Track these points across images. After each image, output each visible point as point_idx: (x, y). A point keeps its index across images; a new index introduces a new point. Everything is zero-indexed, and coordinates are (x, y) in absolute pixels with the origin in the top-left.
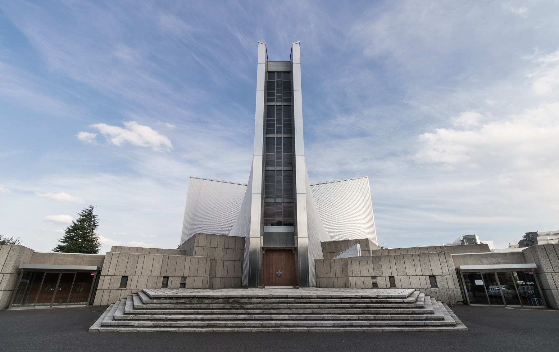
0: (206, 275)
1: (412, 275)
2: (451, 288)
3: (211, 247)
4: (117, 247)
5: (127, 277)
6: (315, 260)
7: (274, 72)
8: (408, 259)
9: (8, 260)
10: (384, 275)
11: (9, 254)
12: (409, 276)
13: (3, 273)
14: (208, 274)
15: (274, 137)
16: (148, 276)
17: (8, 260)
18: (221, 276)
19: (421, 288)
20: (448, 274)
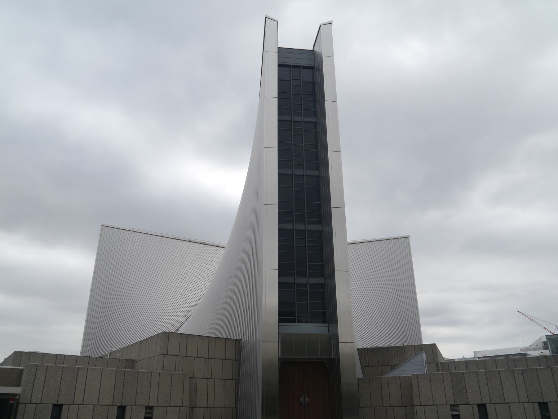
1: (513, 401)
4: (22, 353)
10: (469, 403)
12: (508, 403)
16: (94, 405)
20: (519, 402)
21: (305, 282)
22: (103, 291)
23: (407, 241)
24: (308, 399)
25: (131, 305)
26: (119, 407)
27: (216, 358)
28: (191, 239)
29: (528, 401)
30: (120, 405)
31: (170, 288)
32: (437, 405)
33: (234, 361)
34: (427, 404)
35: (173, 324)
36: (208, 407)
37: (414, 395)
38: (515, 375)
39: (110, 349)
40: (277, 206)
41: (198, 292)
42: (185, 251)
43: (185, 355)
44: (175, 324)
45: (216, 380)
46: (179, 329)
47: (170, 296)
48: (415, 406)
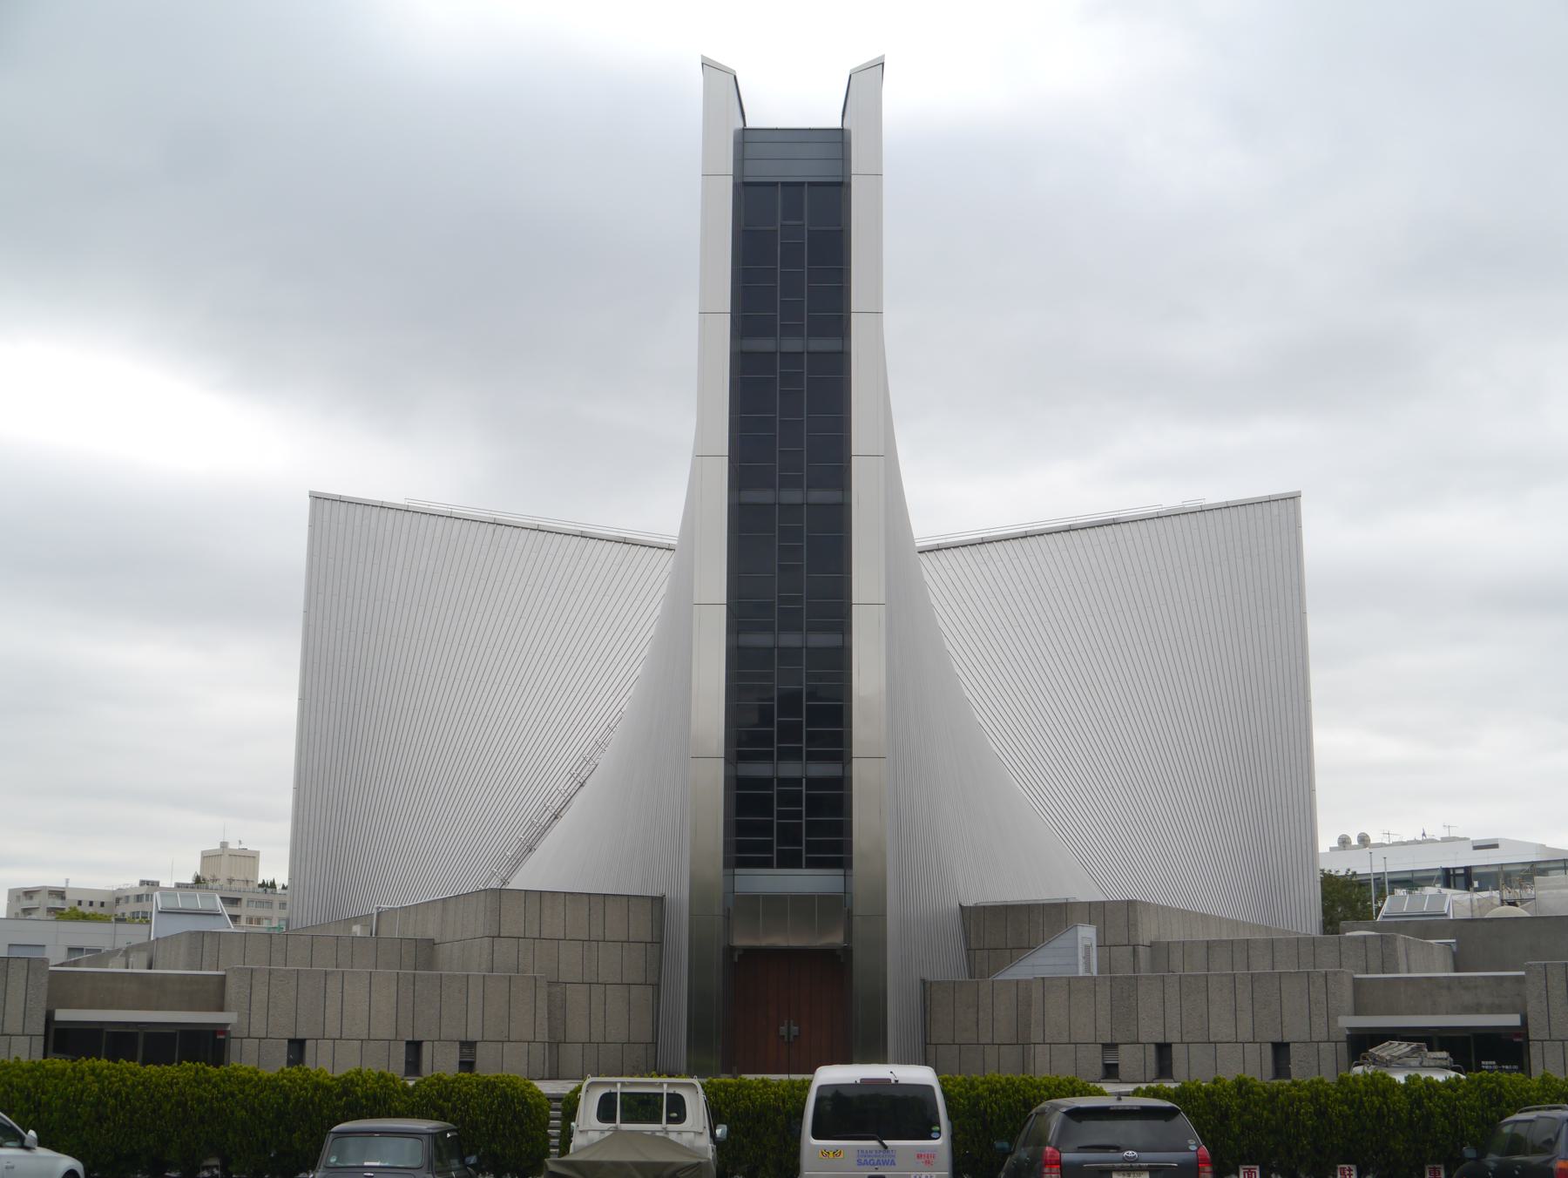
0: (537, 1035)
3: (542, 937)
5: (1288, 1045)
6: (924, 982)
7: (802, 184)
9: (31, 1001)
10: (1140, 1040)
11: (29, 983)
13: (28, 1035)
14: (543, 1035)
15: (801, 350)
17: (31, 1001)
21: (798, 644)
22: (333, 700)
25: (420, 740)
26: (408, 1043)
29: (1252, 1040)
30: (411, 1039)
31: (530, 686)
33: (648, 945)
35: (542, 798)
37: (1033, 1021)
39: (379, 905)
40: (725, 606)
41: (612, 698)
42: (570, 569)
43: (538, 936)
44: (547, 799)
46: (561, 814)
47: (476, 814)
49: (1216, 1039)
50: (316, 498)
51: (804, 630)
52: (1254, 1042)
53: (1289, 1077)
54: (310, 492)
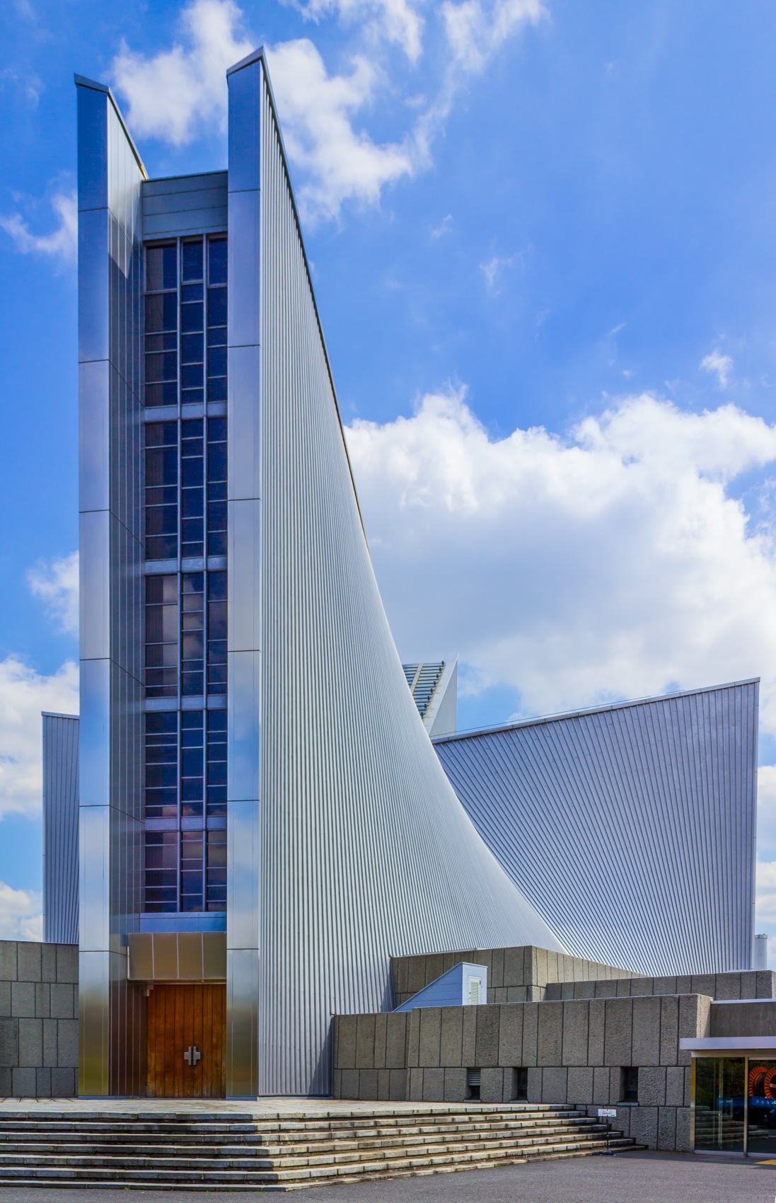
2: (673, 1104)
5: (637, 1068)
8: (576, 1016)
12: (567, 1067)
13: (591, 1067)
18: (37, 1062)
19: (592, 1104)
23: (751, 692)
24: (199, 1053)
27: (58, 982)
28: (580, 711)
29: (602, 1064)
32: (445, 1067)
34: (430, 1066)
36: (45, 1066)
38: (590, 1011)
45: (59, 1021)
48: (409, 1069)
49: (569, 1063)
50: (47, 717)
51: (205, 692)
52: (604, 1066)
53: (636, 1101)
54: (42, 712)
